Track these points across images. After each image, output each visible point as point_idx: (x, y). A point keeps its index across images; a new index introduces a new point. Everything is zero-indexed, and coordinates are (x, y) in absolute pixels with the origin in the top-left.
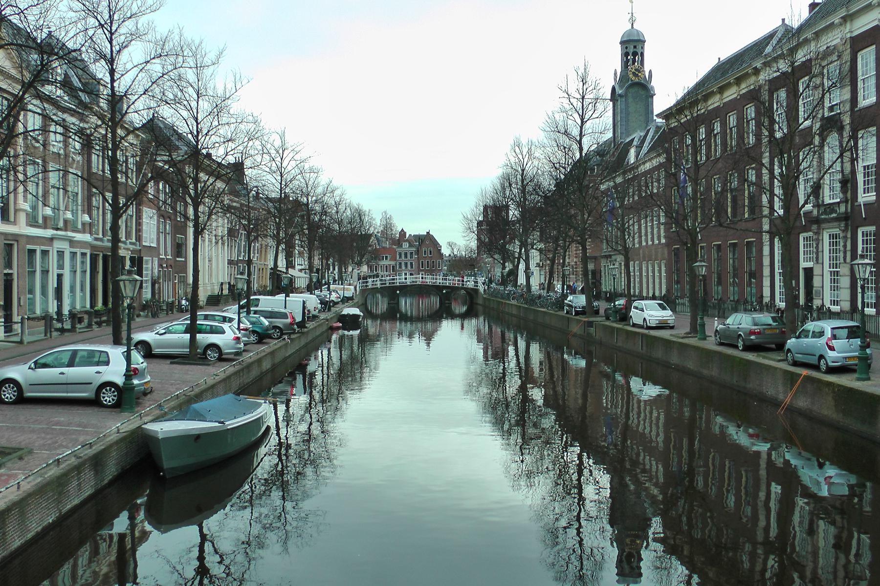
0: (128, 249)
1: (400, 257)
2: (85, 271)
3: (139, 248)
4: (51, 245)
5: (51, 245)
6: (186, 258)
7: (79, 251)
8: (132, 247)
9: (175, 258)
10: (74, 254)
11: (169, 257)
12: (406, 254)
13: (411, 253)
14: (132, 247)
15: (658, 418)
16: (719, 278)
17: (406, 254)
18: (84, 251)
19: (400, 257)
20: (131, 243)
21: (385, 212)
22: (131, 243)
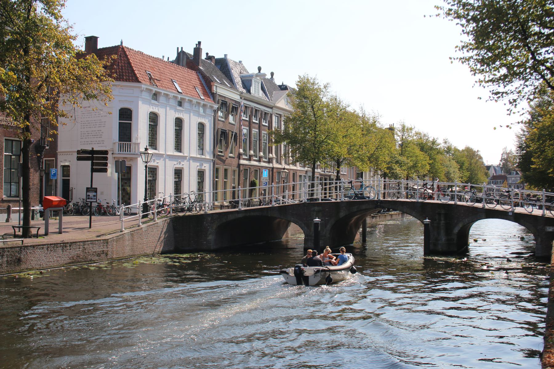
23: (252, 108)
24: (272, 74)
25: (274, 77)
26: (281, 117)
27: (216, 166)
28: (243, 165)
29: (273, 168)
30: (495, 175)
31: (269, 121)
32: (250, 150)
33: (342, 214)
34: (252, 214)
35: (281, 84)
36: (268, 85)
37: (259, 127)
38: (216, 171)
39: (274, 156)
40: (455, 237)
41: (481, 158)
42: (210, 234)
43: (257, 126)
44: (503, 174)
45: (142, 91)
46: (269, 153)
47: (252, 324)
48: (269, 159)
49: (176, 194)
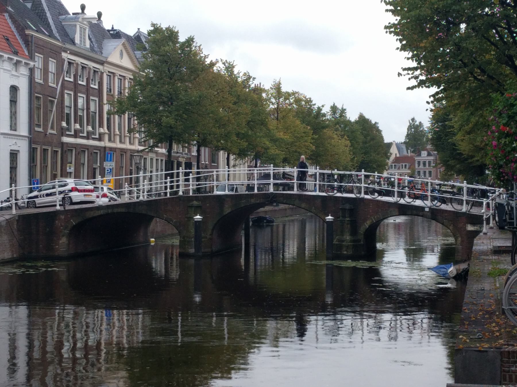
0: (183, 157)
1: (419, 165)
2: (123, 167)
3: (189, 156)
4: (148, 155)
5: (148, 155)
6: (218, 163)
7: (160, 159)
8: (186, 156)
9: (210, 163)
10: (157, 160)
11: (207, 163)
12: (424, 164)
13: (430, 163)
14: (186, 156)
15: (102, 317)
16: (235, 177)
17: (424, 164)
18: (162, 158)
19: (419, 165)
20: (185, 154)
21: (413, 120)
22: (185, 154)
23: (77, 64)
24: (100, 14)
25: (102, 19)
26: (114, 76)
27: (34, 146)
28: (67, 143)
29: (105, 148)
30: (398, 155)
31: (99, 83)
32: (88, 125)
33: (227, 210)
34: (116, 210)
35: (110, 28)
36: (100, 34)
37: (87, 90)
38: (32, 152)
39: (107, 131)
40: (361, 237)
41: (379, 131)
42: (63, 236)
43: (84, 90)
44: (409, 154)
45: (3, 61)
46: (100, 127)
47: (429, 269)
48: (100, 134)
49: (30, 184)
